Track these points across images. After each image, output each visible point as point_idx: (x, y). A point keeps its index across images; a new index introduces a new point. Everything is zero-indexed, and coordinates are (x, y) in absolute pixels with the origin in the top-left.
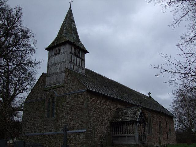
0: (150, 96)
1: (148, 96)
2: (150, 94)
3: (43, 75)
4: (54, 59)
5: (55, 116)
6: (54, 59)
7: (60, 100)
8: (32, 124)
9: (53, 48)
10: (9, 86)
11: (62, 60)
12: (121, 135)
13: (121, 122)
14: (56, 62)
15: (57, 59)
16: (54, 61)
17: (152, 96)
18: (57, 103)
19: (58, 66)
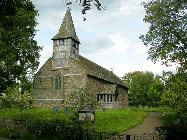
0: (112, 71)
1: (111, 71)
2: (112, 69)
3: (50, 59)
4: (59, 48)
5: (62, 89)
6: (59, 48)
7: (66, 79)
8: (43, 93)
9: (58, 40)
10: (176, 123)
11: (65, 50)
12: (108, 102)
13: (104, 94)
14: (60, 51)
15: (61, 48)
16: (59, 50)
17: (114, 72)
18: (63, 80)
19: (63, 54)
